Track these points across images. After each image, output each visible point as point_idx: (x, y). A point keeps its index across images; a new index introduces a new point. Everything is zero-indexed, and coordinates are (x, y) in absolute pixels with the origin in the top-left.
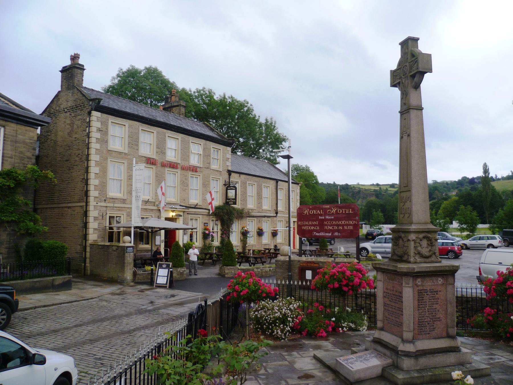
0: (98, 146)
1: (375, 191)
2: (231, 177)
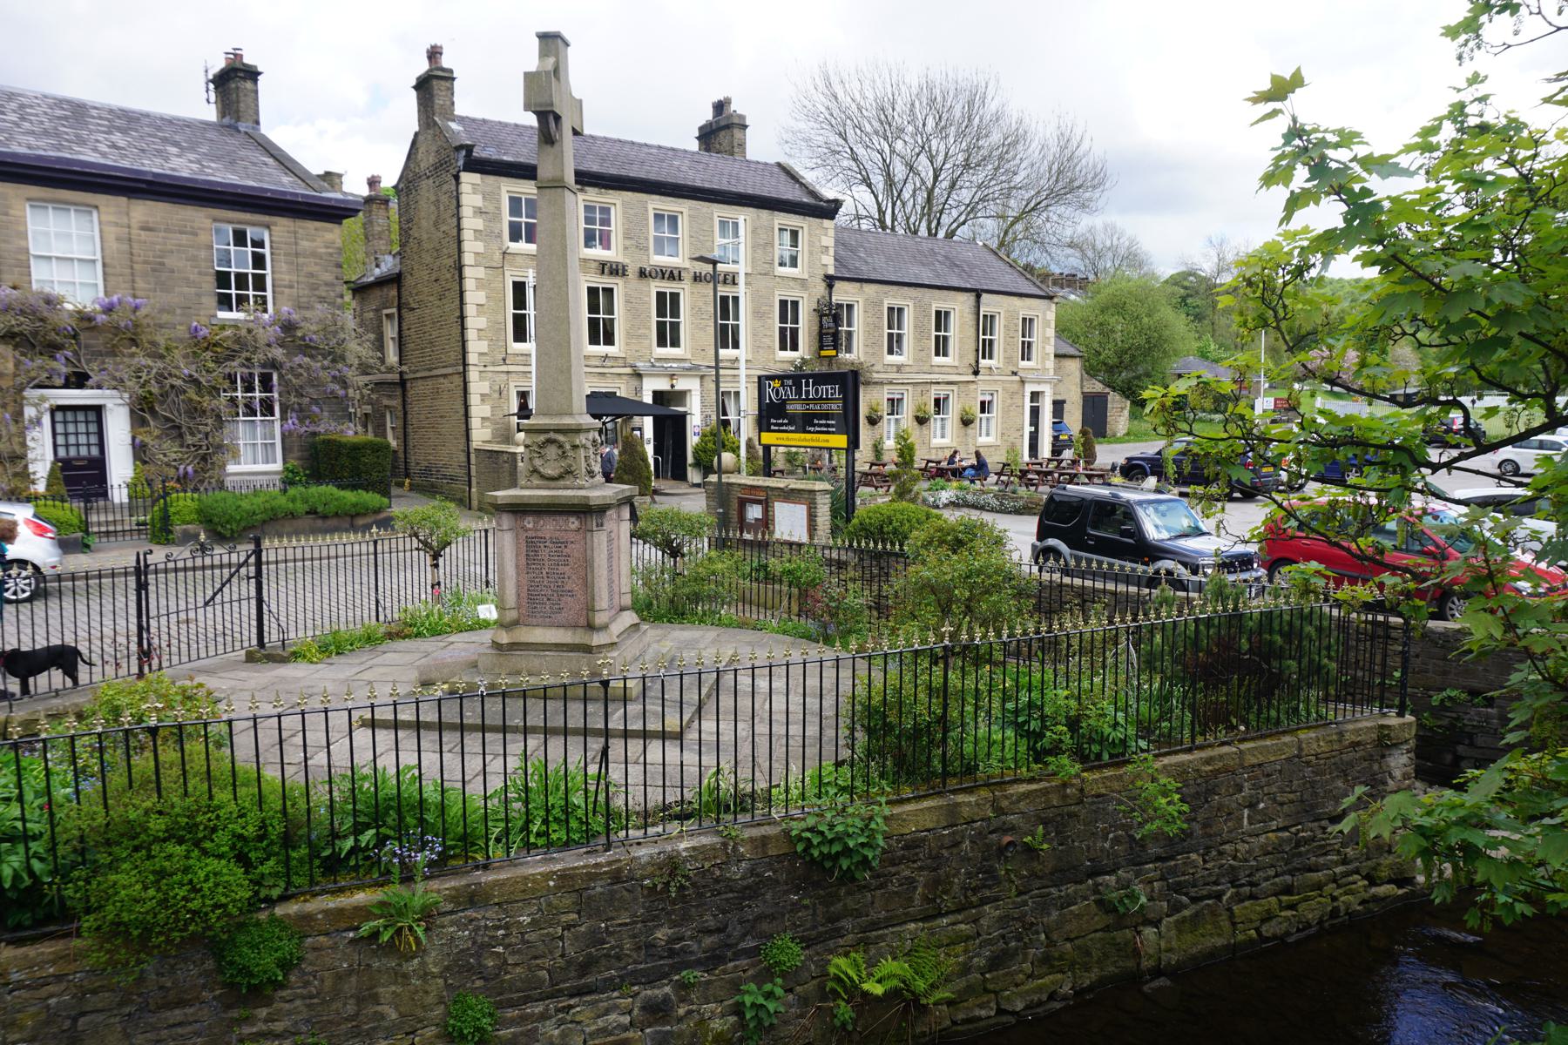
0: (479, 247)
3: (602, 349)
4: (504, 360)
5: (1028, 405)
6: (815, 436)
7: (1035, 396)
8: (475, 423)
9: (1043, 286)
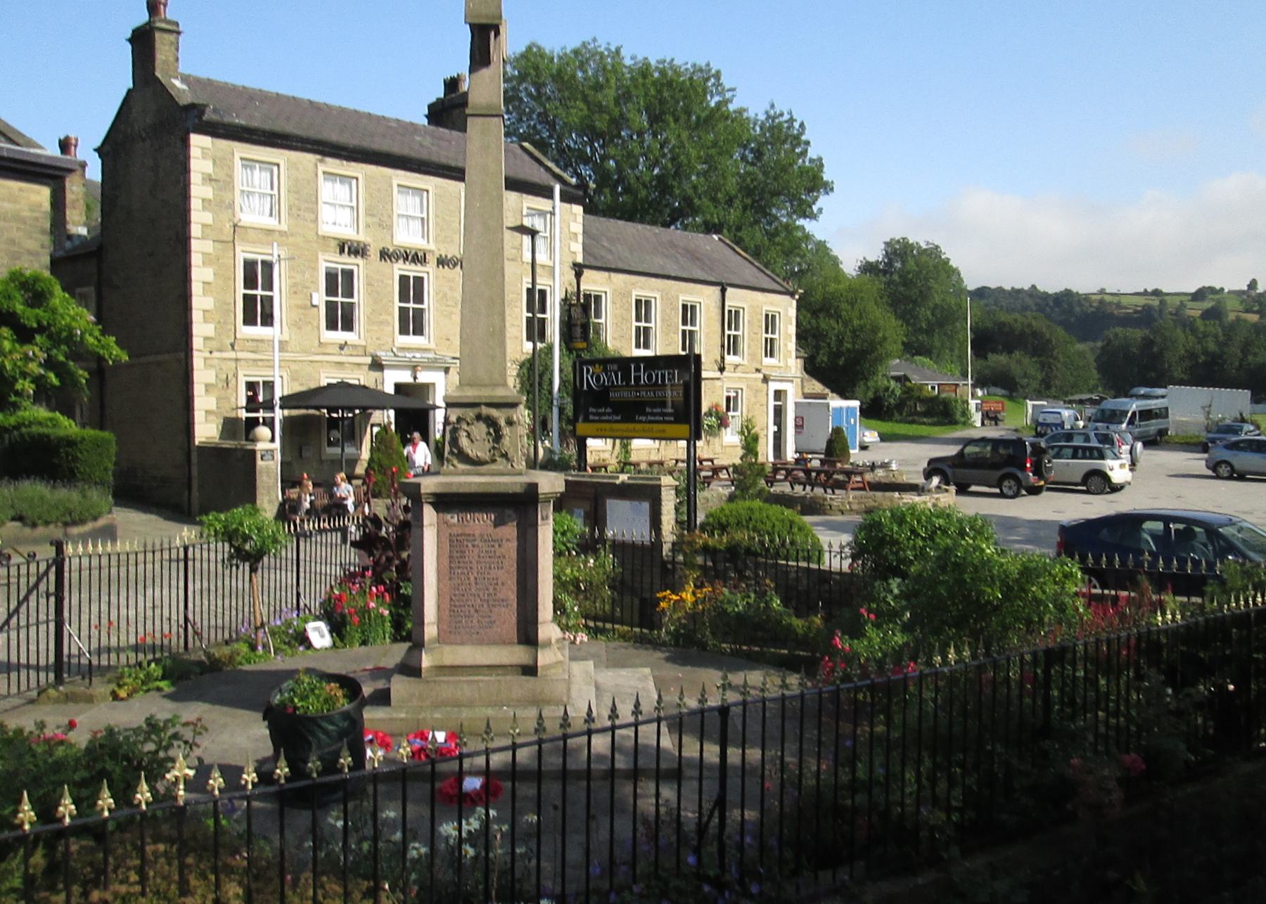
0: (208, 218)
1: (1147, 309)
2: (583, 279)
3: (340, 336)
4: (233, 346)
5: (772, 403)
6: (647, 426)
7: (779, 394)
8: (199, 416)
9: (785, 284)
